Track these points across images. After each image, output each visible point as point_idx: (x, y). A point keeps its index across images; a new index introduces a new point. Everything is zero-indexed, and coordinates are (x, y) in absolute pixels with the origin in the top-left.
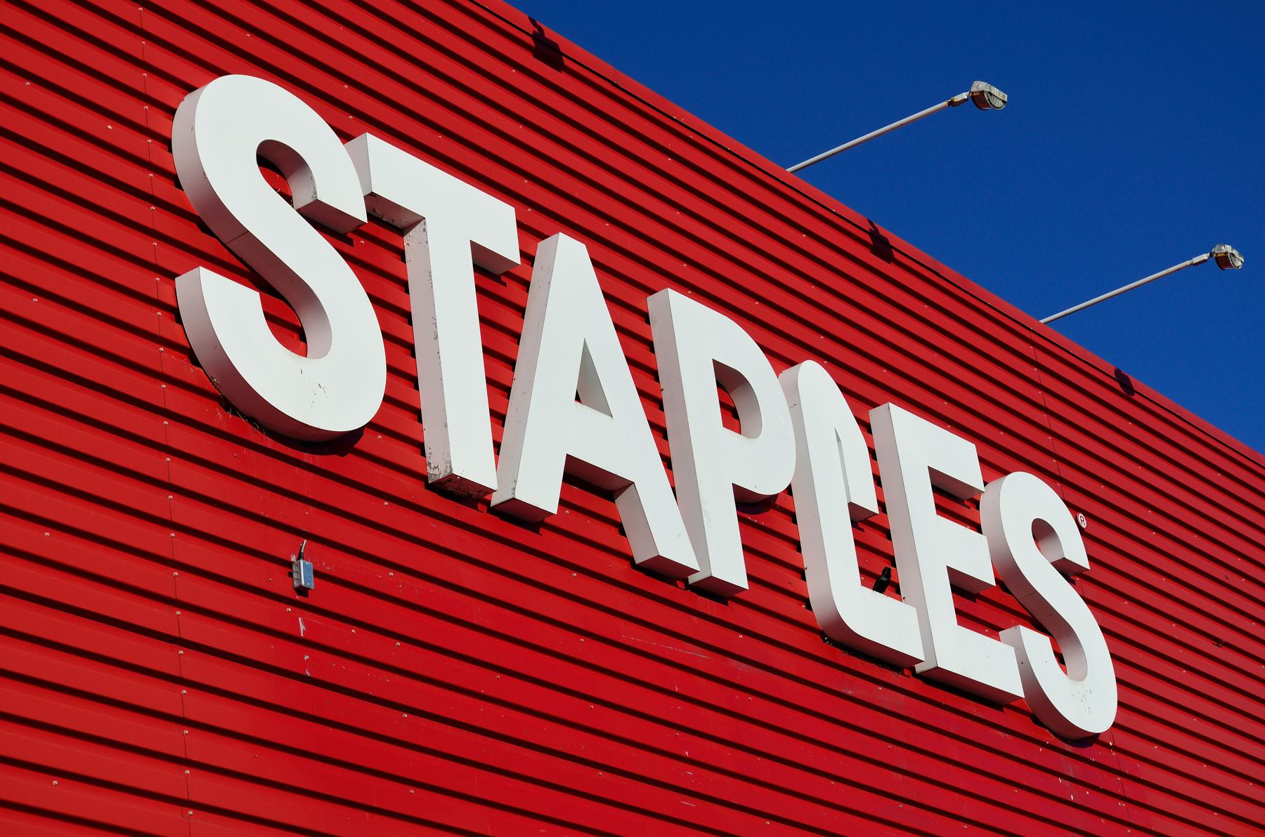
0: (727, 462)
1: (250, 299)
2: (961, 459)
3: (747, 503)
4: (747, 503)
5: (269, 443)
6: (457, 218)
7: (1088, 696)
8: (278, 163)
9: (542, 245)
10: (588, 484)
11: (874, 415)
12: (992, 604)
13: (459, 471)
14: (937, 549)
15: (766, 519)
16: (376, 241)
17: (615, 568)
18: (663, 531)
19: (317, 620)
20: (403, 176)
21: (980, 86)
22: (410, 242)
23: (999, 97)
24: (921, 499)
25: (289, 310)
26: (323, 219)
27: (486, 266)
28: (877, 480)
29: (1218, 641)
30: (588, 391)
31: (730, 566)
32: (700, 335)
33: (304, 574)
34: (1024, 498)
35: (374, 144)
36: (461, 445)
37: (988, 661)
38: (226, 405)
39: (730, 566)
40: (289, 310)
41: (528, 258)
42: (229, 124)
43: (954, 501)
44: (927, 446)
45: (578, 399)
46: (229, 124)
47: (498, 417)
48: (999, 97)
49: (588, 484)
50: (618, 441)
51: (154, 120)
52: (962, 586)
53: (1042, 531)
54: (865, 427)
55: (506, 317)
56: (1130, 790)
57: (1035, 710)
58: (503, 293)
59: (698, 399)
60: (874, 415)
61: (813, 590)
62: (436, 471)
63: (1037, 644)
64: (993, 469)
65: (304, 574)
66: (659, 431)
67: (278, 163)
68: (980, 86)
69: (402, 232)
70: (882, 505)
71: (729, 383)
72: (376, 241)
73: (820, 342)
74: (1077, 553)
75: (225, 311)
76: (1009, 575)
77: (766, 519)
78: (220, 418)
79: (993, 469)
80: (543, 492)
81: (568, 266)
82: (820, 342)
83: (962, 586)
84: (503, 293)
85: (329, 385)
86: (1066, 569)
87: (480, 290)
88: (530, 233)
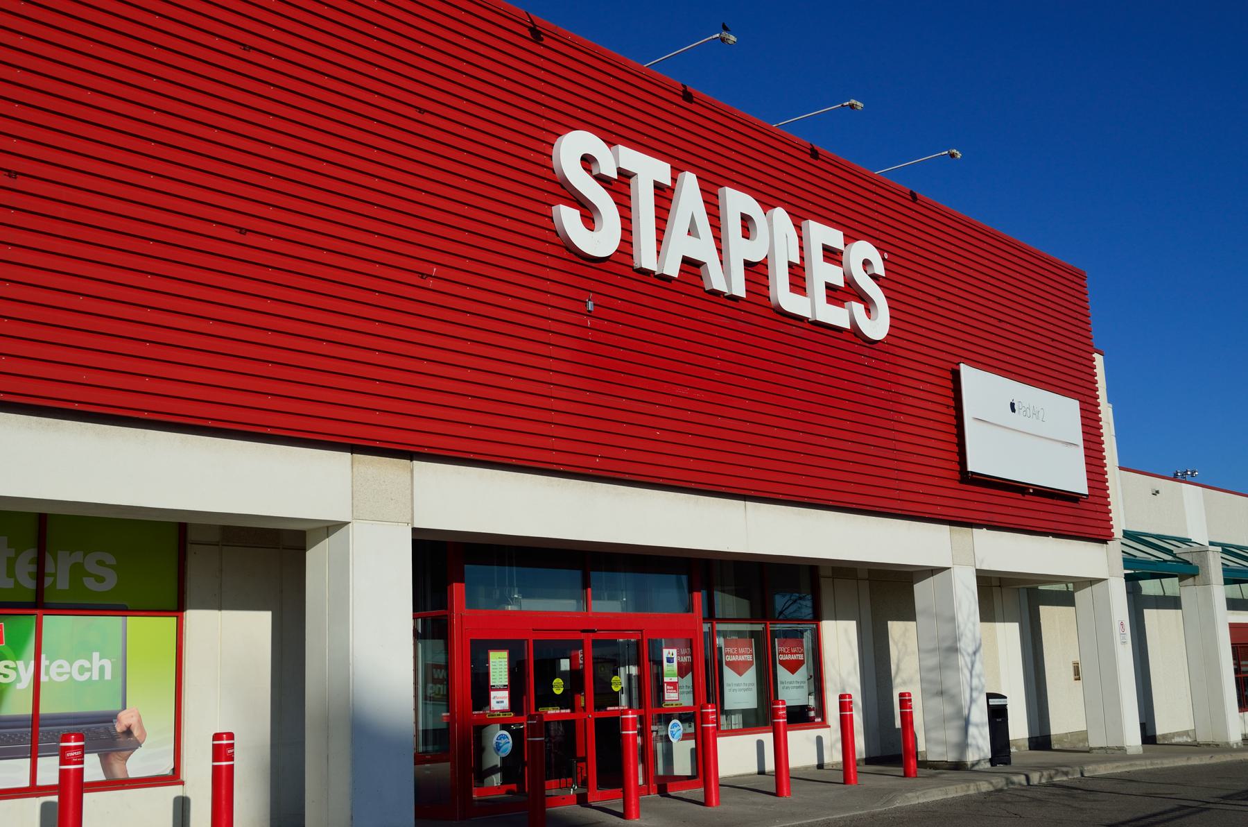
0: (741, 250)
1: (577, 213)
2: (835, 238)
3: (748, 264)
4: (748, 264)
5: (581, 261)
6: (649, 170)
7: (877, 327)
8: (588, 162)
9: (680, 175)
10: (691, 265)
11: (804, 224)
12: (836, 295)
13: (644, 266)
14: (823, 274)
15: (756, 272)
16: (620, 186)
17: (697, 292)
18: (716, 280)
19: (594, 320)
20: (630, 158)
21: (853, 101)
22: (632, 181)
23: (860, 105)
24: (816, 254)
25: (589, 216)
26: (602, 180)
27: (658, 187)
28: (801, 248)
29: (939, 298)
30: (692, 231)
31: (739, 290)
32: (736, 202)
33: (590, 306)
34: (863, 250)
35: (622, 149)
36: (646, 258)
37: (837, 316)
38: (567, 249)
39: (739, 290)
40: (589, 216)
41: (674, 180)
42: (572, 149)
43: (831, 255)
44: (822, 234)
45: (689, 233)
46: (572, 149)
47: (659, 242)
48: (860, 105)
49: (691, 265)
50: (703, 249)
51: (542, 147)
52: (830, 287)
53: (866, 263)
54: (798, 228)
55: (664, 203)
56: (891, 359)
57: (855, 331)
58: (664, 196)
59: (733, 226)
60: (804, 224)
61: (771, 296)
62: (637, 266)
63: (858, 308)
64: (849, 239)
65: (590, 306)
66: (720, 251)
67: (588, 162)
68: (853, 101)
69: (630, 177)
70: (802, 258)
71: (746, 220)
72: (620, 186)
73: (785, 197)
74: (879, 269)
75: (568, 218)
76: (850, 281)
77: (756, 272)
78: (565, 254)
79: (849, 239)
80: (672, 269)
81: (690, 182)
82: (785, 197)
83: (830, 287)
84: (664, 196)
85: (599, 242)
86: (874, 277)
87: (655, 194)
88: (676, 171)
